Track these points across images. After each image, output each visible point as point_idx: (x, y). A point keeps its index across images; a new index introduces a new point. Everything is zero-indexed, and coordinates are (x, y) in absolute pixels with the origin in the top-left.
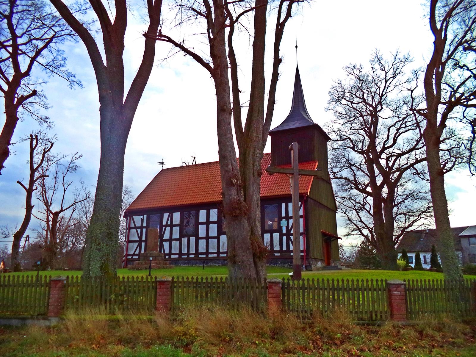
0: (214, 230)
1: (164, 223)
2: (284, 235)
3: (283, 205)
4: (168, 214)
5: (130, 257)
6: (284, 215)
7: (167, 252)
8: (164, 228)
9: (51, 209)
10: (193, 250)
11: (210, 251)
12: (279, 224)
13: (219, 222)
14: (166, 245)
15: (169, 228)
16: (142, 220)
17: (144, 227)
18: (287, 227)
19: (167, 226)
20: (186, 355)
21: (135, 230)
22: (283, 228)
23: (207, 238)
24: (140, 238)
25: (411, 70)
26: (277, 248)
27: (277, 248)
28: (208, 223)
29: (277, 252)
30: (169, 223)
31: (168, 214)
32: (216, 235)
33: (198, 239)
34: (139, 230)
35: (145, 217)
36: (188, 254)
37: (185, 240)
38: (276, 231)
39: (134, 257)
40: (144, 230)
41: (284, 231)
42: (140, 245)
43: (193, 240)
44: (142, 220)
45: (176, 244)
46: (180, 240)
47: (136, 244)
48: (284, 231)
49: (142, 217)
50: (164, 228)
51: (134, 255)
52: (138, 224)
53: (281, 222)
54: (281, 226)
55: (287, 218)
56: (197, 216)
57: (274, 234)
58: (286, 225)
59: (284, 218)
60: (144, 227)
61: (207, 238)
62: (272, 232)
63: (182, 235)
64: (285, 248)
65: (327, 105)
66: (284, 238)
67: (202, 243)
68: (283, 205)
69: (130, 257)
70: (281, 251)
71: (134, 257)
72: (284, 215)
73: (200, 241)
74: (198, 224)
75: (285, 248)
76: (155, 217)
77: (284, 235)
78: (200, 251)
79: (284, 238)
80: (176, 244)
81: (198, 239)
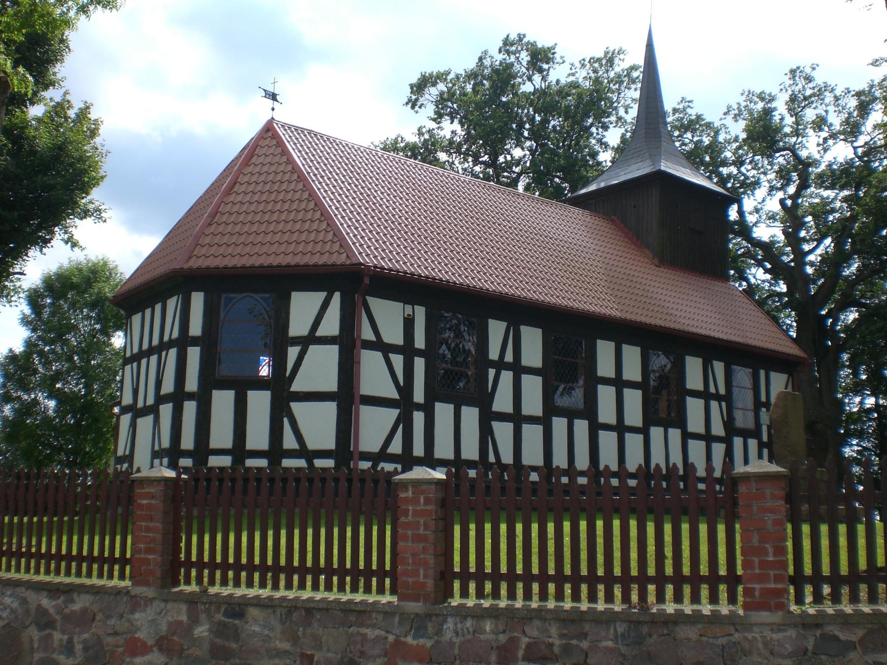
1: (494, 354)
4: (504, 325)
5: (365, 465)
7: (507, 458)
10: (582, 462)
15: (173, 352)
17: (195, 341)
19: (500, 365)
20: (71, 661)
24: (406, 390)
33: (595, 428)
37: (559, 424)
38: (580, 415)
42: (405, 421)
43: (582, 426)
44: (409, 324)
46: (545, 422)
51: (383, 455)
52: (394, 335)
60: (195, 341)
62: (571, 415)
67: (608, 441)
69: (365, 465)
73: (603, 435)
74: (594, 381)
76: (245, 304)
80: (532, 434)
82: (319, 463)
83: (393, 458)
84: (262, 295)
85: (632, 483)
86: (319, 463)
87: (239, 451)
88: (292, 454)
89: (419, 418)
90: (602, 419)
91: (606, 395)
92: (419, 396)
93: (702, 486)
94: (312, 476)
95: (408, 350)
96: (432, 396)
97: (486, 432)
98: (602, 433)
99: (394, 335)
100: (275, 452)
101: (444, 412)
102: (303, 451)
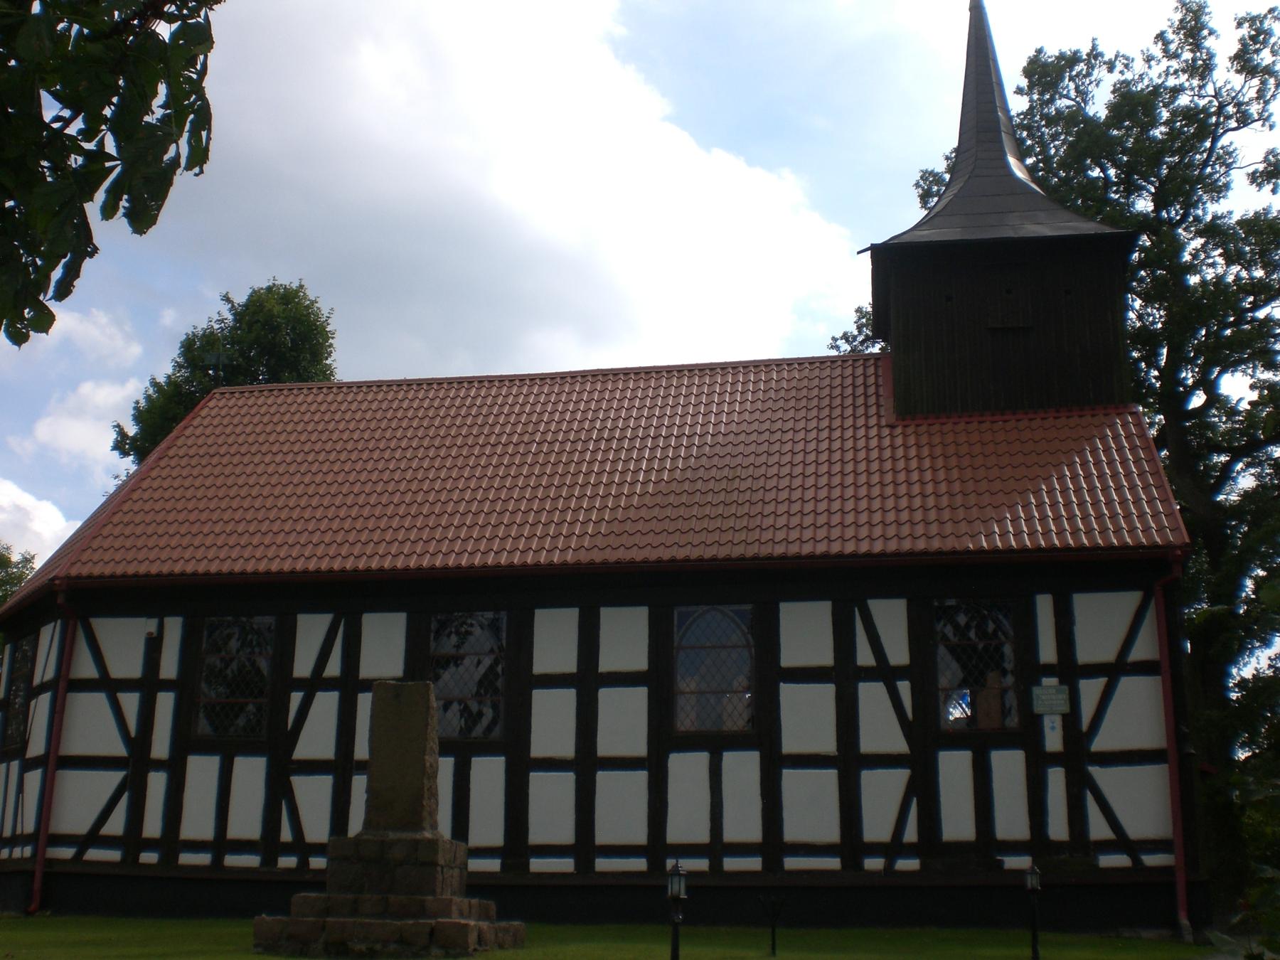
0: (624, 721)
1: (303, 667)
2: (1055, 759)
3: (1044, 606)
4: (325, 620)
5: (67, 853)
6: (1048, 652)
8: (296, 698)
11: (792, 833)
13: (658, 679)
16: (154, 646)
18: (1071, 720)
19: (316, 683)
21: (99, 700)
22: (1047, 722)
23: (849, 761)
24: (139, 742)
26: (1011, 821)
28: (587, 681)
29: (1014, 848)
30: (333, 668)
31: (325, 620)
32: (639, 748)
33: (775, 765)
34: (130, 702)
35: (174, 628)
36: (221, 844)
38: (738, 742)
39: (93, 854)
40: (165, 703)
41: (1053, 740)
42: (134, 789)
43: (743, 769)
44: (154, 646)
47: (899, 778)
48: (1053, 740)
49: (151, 625)
50: (296, 698)
51: (94, 838)
54: (1038, 708)
57: (729, 758)
58: (1066, 708)
59: (1048, 670)
64: (1058, 828)
66: (1056, 779)
68: (1044, 606)
69: (67, 853)
70: (1038, 843)
71: (93, 854)
72: (1048, 652)
73: (539, 782)
74: (769, 675)
75: (1058, 828)
76: (716, 629)
77: (1055, 759)
79: (1056, 779)
81: (775, 765)
82: (1150, 860)
83: (109, 842)
84: (736, 607)
85: (318, 863)
86: (1150, 860)
87: (171, 841)
88: (287, 849)
89: (157, 783)
90: (539, 749)
91: (1049, 693)
92: (161, 747)
93: (1019, 862)
94: (216, 877)
95: (148, 685)
96: (184, 744)
97: (278, 793)
98: (789, 775)
99: (126, 664)
100: (268, 845)
101: (202, 771)
102: (1121, 842)
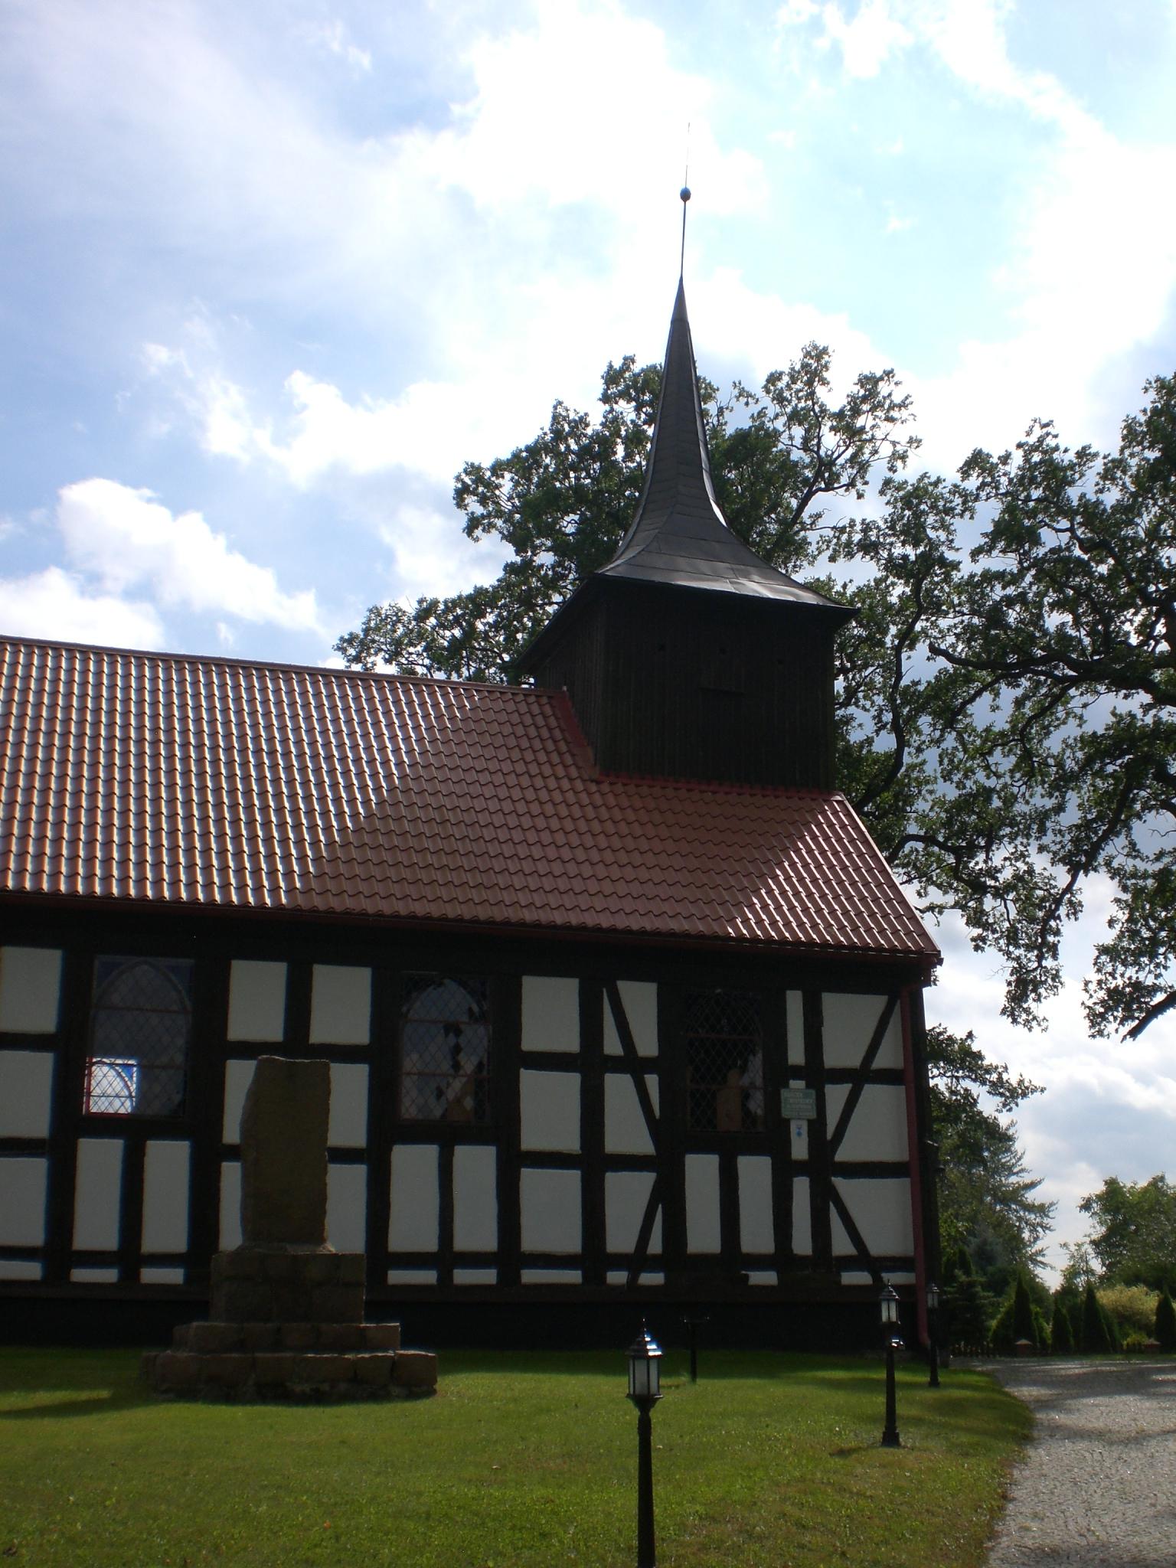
2: (801, 1168)
3: (794, 1001)
5: (617, 1277)
6: (796, 1055)
9: (895, 746)
10: (477, 1230)
12: (773, 1102)
14: (346, 1186)
18: (816, 1126)
25: (460, 467)
26: (757, 1237)
27: (757, 1237)
29: (760, 1262)
37: (701, 1172)
41: (800, 1149)
43: (476, 1164)
45: (628, 1197)
46: (375, 1159)
48: (800, 1149)
51: (637, 1261)
53: (784, 1093)
54: (785, 1114)
55: (817, 1075)
56: (507, 1018)
59: (797, 1072)
61: (593, 1162)
63: (388, 1127)
64: (802, 1243)
65: (462, 519)
66: (801, 1187)
68: (794, 1001)
70: (782, 1258)
72: (796, 1055)
74: (508, 1059)
75: (802, 1243)
77: (801, 1168)
78: (399, 1240)
79: (801, 1187)
